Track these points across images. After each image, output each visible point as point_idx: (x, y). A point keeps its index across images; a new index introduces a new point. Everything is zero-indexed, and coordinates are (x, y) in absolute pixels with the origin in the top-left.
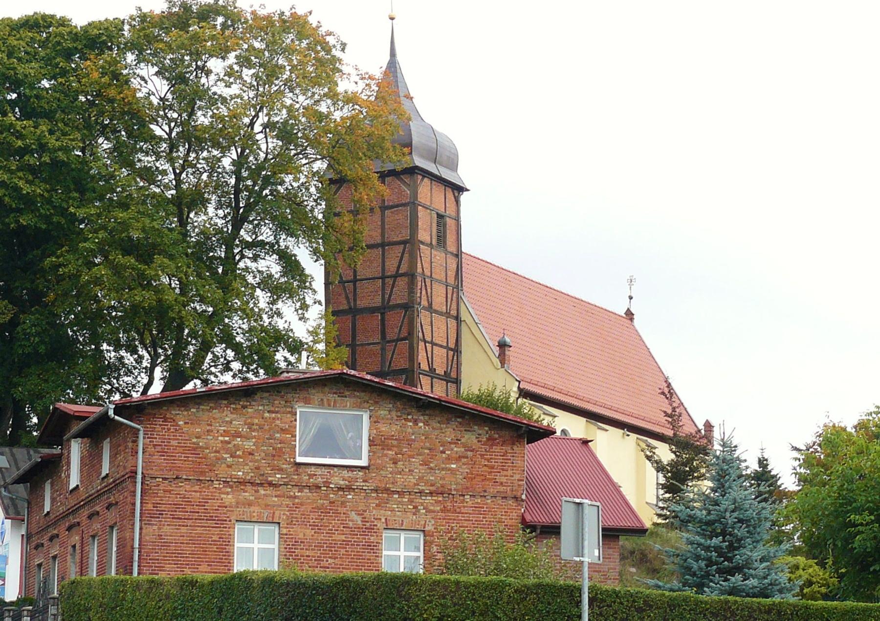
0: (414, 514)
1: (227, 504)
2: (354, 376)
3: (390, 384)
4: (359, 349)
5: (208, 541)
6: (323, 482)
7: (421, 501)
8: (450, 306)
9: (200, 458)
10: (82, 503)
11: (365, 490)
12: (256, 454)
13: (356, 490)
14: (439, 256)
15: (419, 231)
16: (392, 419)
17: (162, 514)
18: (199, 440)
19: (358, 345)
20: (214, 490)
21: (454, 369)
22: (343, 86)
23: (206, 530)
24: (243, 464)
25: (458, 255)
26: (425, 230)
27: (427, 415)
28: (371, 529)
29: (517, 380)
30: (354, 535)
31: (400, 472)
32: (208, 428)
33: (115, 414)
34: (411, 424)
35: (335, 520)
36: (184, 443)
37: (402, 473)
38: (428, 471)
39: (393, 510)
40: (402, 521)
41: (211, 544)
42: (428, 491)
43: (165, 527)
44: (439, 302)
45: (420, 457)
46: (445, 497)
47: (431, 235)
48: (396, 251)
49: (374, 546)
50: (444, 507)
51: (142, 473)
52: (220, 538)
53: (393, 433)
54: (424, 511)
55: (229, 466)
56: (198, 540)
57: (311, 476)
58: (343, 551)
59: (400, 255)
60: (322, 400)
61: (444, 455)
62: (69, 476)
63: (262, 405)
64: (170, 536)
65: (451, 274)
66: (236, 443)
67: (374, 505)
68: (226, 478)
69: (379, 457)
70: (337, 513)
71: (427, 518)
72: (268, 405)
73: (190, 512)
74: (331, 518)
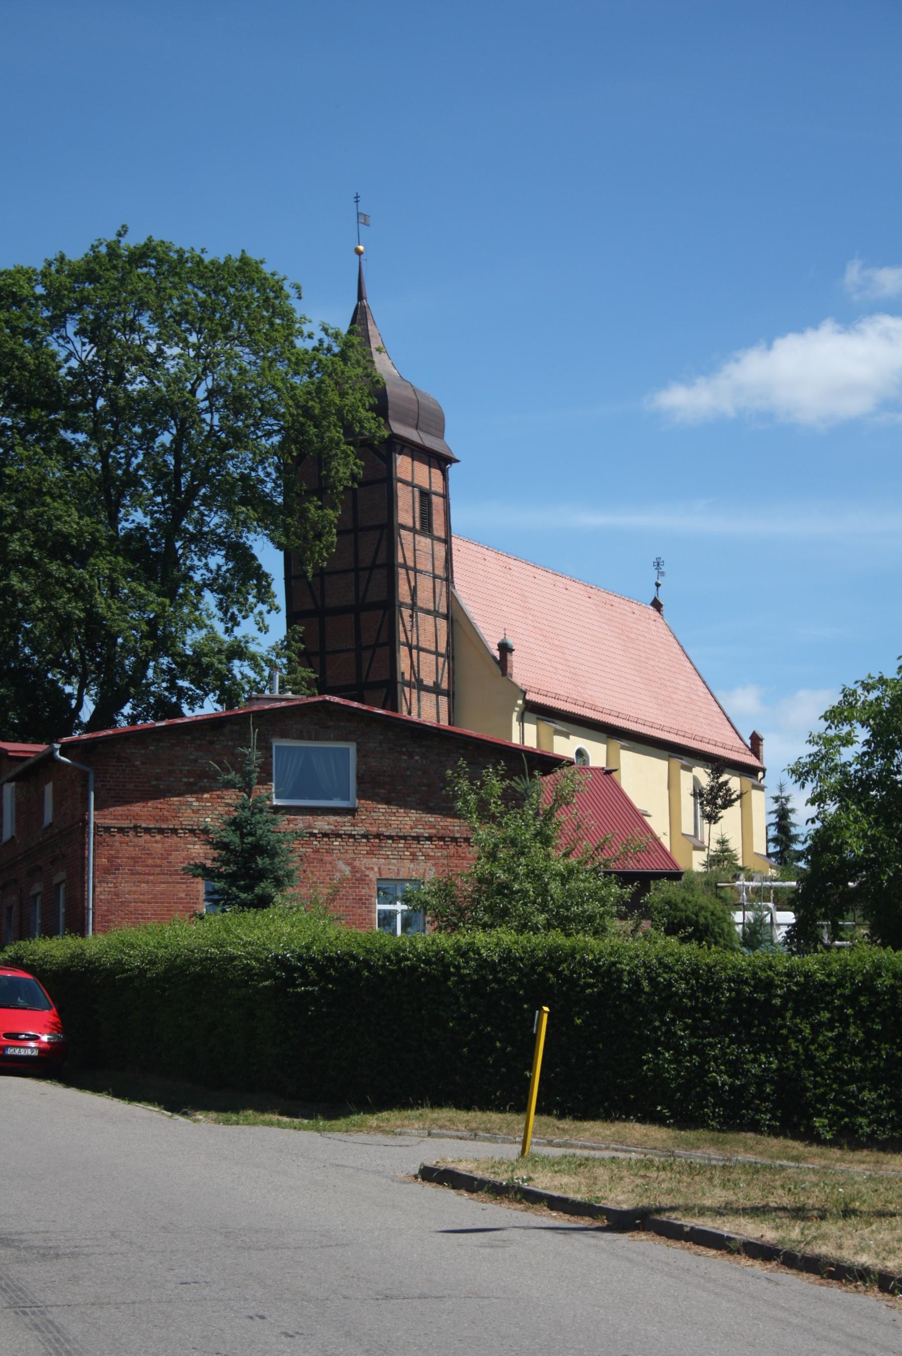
0: (412, 860)
2: (338, 704)
10: (19, 858)
14: (424, 542)
24: (212, 808)
26: (407, 511)
32: (169, 768)
34: (405, 757)
37: (397, 814)
41: (176, 903)
42: (427, 835)
47: (414, 517)
54: (423, 858)
55: (195, 812)
66: (202, 784)
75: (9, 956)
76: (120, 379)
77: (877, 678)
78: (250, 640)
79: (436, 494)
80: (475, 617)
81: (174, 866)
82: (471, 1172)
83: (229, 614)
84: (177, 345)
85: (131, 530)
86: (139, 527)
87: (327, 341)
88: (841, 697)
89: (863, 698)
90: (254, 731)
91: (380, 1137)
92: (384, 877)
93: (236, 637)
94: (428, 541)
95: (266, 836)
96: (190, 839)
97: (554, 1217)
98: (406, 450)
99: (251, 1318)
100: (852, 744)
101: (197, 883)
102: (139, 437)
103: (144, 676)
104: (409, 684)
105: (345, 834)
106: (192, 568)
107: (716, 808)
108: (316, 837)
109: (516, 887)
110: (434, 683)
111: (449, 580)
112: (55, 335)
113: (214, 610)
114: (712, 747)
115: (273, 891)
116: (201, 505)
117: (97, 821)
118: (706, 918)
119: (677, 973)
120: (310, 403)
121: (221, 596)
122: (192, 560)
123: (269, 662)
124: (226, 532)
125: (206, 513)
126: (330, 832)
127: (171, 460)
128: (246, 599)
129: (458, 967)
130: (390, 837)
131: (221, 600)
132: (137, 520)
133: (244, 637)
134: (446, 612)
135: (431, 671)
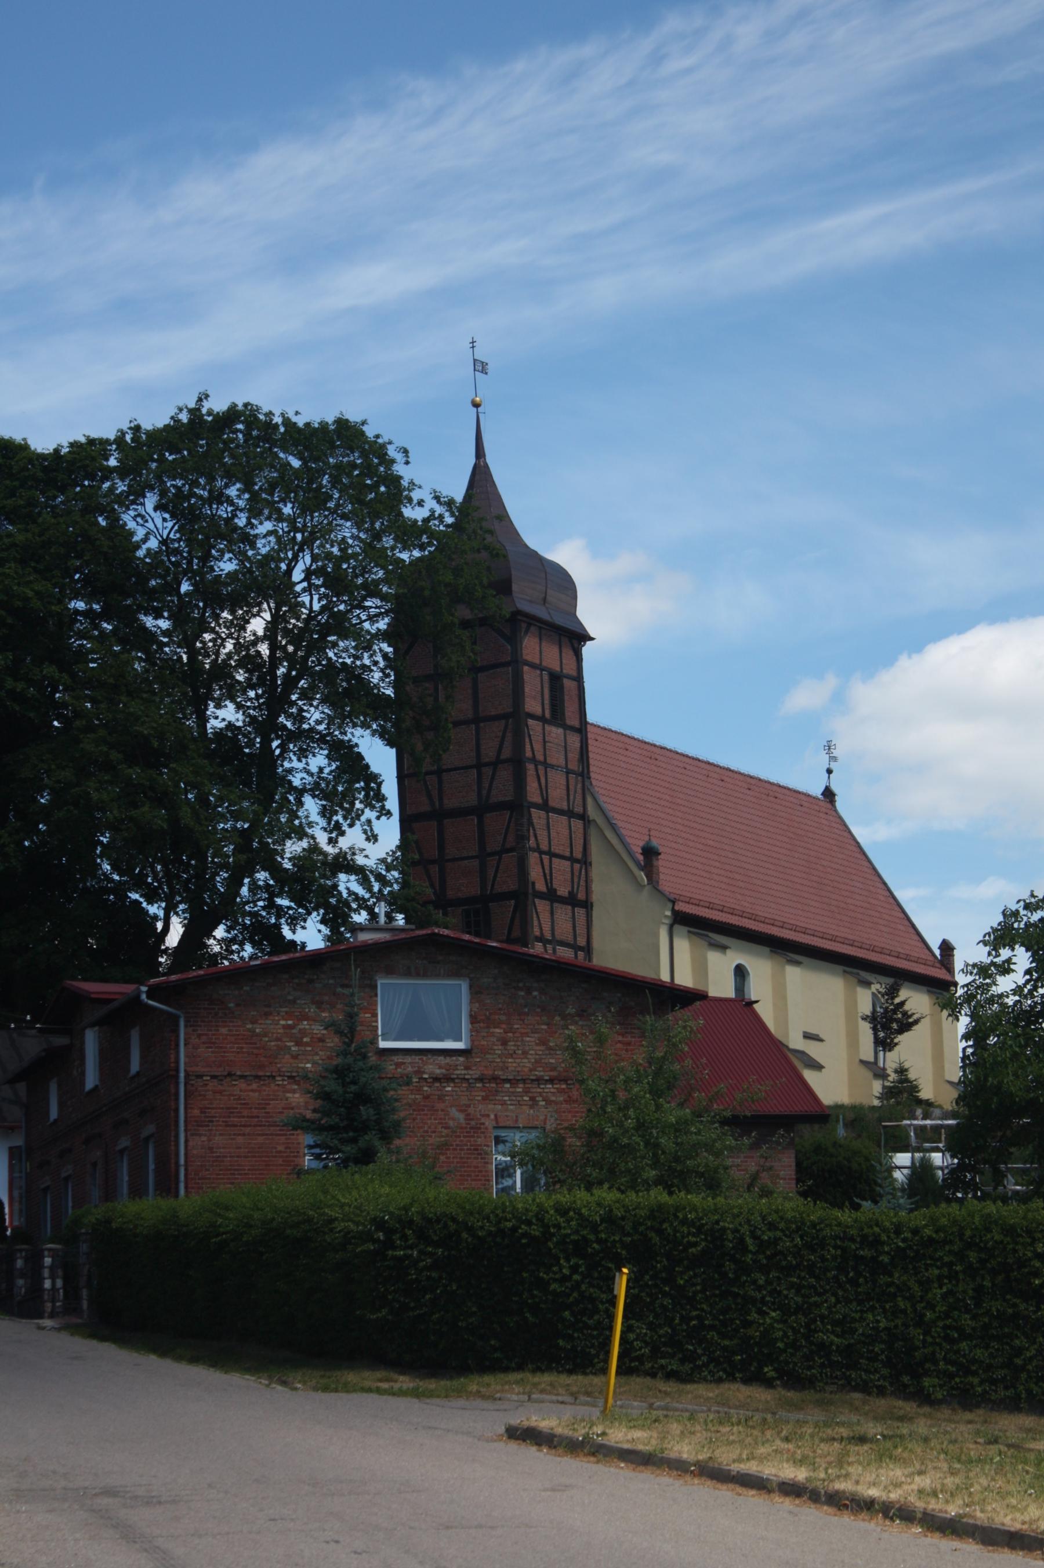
0: (531, 1107)
1: (294, 1104)
2: (447, 937)
3: (494, 944)
7: (539, 1090)
8: (574, 802)
10: (104, 1109)
12: (327, 1040)
13: (457, 1081)
14: (555, 733)
15: (527, 700)
17: (212, 1121)
18: (255, 1026)
19: (449, 860)
20: (276, 1088)
21: (582, 889)
25: (582, 727)
29: (670, 900)
31: (512, 1055)
33: (148, 997)
34: (522, 993)
35: (430, 1119)
36: (236, 1031)
37: (514, 1056)
38: (547, 1052)
39: (504, 1103)
40: (517, 1117)
41: (276, 1157)
42: (547, 1078)
43: (217, 1138)
44: (557, 796)
45: (536, 1035)
46: (570, 1084)
50: (569, 1097)
51: (185, 1071)
53: (500, 1006)
54: (544, 1103)
55: (295, 1057)
57: (398, 1065)
59: (501, 734)
62: (83, 1074)
64: (224, 1148)
65: (574, 756)
67: (480, 1098)
68: (291, 1072)
73: (248, 1117)
75: (97, 1219)
76: (206, 557)
78: (357, 852)
80: (616, 816)
81: (272, 1117)
82: (552, 1429)
83: (333, 823)
84: (269, 518)
85: (221, 729)
86: (230, 726)
87: (439, 510)
88: (1001, 918)
89: (1025, 919)
90: (356, 970)
91: (479, 1403)
92: (501, 1125)
93: (341, 849)
94: (560, 731)
95: (370, 1084)
96: (288, 1087)
97: (622, 1468)
98: (532, 628)
99: (327, 1542)
100: (1008, 973)
101: (298, 1135)
102: (229, 625)
103: (238, 894)
104: (541, 896)
105: (458, 1078)
106: (290, 771)
107: (892, 1033)
108: (427, 1082)
109: (626, 1141)
110: (569, 892)
111: (584, 774)
112: (132, 513)
113: (315, 817)
115: (377, 1143)
116: (299, 699)
117: (189, 1069)
118: (860, 1164)
119: (782, 1231)
121: (324, 803)
122: (291, 760)
123: (380, 878)
125: (305, 708)
126: (441, 1076)
127: (264, 649)
128: (353, 804)
129: (558, 1226)
130: (508, 1081)
131: (324, 806)
132: (228, 719)
133: (350, 848)
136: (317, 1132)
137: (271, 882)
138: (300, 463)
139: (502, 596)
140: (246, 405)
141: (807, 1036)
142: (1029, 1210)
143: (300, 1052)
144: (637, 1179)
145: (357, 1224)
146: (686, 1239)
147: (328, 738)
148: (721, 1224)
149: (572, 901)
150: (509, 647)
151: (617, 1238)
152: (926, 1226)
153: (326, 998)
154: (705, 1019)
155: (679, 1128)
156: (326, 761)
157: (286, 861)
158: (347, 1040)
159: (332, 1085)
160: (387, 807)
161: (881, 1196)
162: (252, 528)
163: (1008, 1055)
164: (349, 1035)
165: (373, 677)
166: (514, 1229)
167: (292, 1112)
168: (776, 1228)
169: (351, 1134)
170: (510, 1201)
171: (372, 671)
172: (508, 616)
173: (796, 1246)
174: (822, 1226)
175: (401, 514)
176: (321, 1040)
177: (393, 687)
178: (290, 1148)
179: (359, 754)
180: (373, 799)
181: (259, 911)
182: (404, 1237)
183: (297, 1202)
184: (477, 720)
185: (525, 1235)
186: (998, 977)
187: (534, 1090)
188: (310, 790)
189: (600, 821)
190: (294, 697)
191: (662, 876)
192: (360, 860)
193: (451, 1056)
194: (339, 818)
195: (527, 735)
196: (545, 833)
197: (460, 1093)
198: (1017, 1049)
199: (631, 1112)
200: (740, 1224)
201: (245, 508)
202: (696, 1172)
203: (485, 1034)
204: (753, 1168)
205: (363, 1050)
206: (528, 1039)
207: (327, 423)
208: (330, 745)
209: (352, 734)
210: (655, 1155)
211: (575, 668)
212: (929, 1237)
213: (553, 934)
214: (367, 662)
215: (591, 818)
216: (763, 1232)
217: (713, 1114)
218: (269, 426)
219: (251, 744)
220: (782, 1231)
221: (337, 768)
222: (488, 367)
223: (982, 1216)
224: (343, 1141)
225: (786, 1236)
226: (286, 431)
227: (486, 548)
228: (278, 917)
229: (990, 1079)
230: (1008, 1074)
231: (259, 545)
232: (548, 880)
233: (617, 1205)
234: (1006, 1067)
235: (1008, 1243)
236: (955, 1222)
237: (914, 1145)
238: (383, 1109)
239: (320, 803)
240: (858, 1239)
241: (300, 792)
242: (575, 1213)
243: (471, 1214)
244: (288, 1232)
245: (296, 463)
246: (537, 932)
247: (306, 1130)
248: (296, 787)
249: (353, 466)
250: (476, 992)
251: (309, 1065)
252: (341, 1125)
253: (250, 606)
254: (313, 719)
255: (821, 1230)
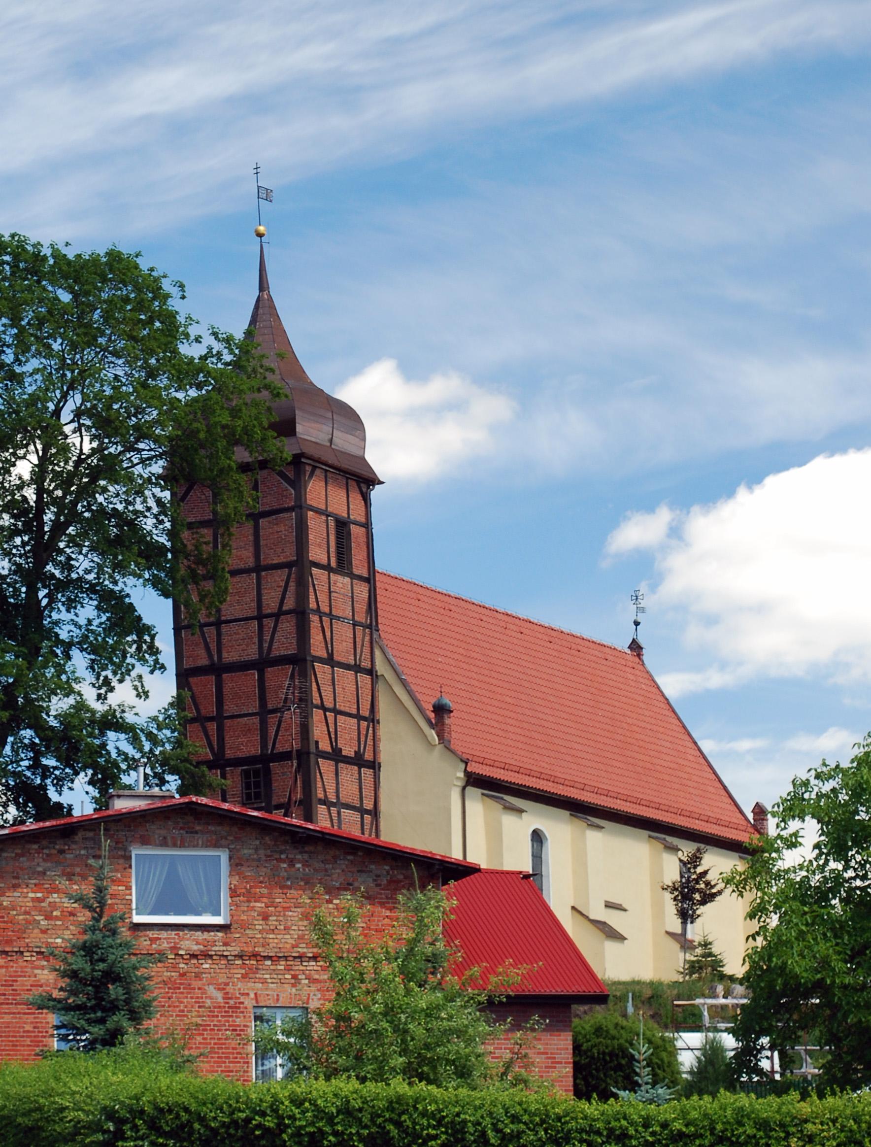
0: (294, 985)
1: (43, 981)
2: (206, 805)
4: (228, 723)
5: (19, 1032)
6: (171, 948)
7: (301, 968)
8: (361, 656)
9: (4, 922)
11: (227, 956)
12: (79, 914)
13: (214, 957)
14: (342, 582)
16: (259, 860)
20: (25, 964)
21: (369, 748)
22: (190, 350)
23: (16, 1018)
24: (63, 927)
25: (370, 579)
26: (320, 546)
27: (306, 852)
28: (236, 1008)
29: (462, 760)
30: (213, 1016)
34: (285, 866)
35: (187, 997)
39: (264, 982)
41: (23, 1037)
42: (311, 955)
44: (343, 651)
45: (299, 910)
48: (277, 579)
49: (241, 1030)
52: (35, 1027)
53: (261, 879)
54: (307, 981)
55: (44, 932)
56: (5, 1032)
57: (153, 940)
58: (199, 1039)
59: (283, 583)
60: (165, 838)
61: (331, 906)
63: (85, 848)
65: (361, 606)
67: (239, 976)
69: (243, 912)
70: (189, 987)
71: (311, 991)
72: (92, 848)
74: (181, 996)
77: (833, 766)
78: (127, 709)
79: (356, 523)
83: (102, 678)
87: (217, 346)
89: (816, 789)
90: (106, 841)
92: (260, 1004)
94: (347, 580)
98: (318, 472)
100: (796, 847)
101: (46, 1014)
106: (57, 623)
107: (693, 903)
110: (355, 752)
111: (372, 626)
114: (703, 823)
116: (68, 546)
119: (525, 1123)
120: (195, 425)
121: (93, 657)
123: (150, 736)
124: (98, 578)
125: (74, 556)
126: (198, 953)
127: (30, 493)
129: (292, 1118)
131: (93, 661)
134: (369, 666)
135: (351, 739)
136: (63, 1012)
137: (37, 741)
138: (71, 296)
139: (283, 438)
140: (13, 236)
141: (609, 905)
142: (783, 1103)
143: (50, 927)
144: (384, 1066)
145: (87, 1113)
146: (425, 1132)
147: (98, 588)
148: (462, 1116)
149: (358, 761)
150: (293, 492)
151: (354, 1131)
152: (674, 1120)
153: (78, 870)
154: (458, 899)
155: (430, 1013)
156: (95, 613)
157: (52, 718)
158: (96, 915)
159: (79, 963)
160: (161, 661)
161: (640, 1086)
162: (19, 365)
163: (793, 934)
164: (98, 910)
165: (145, 524)
166: (248, 1120)
167: (41, 989)
168: (520, 1121)
169: (99, 1014)
170: (245, 1092)
171: (146, 517)
172: (289, 459)
173: (540, 1139)
174: (568, 1118)
175: (175, 352)
176: (72, 914)
177: (166, 535)
178: (38, 1028)
179: (131, 604)
180: (146, 652)
181: (23, 771)
182: (135, 1128)
183: (29, 1089)
184: (258, 569)
185: (259, 1126)
186: (784, 850)
187: (297, 968)
188: (78, 643)
189: (389, 676)
190: (62, 545)
191: (454, 735)
192: (130, 718)
193: (209, 931)
194: (109, 673)
195: (311, 585)
196: (330, 689)
197: (218, 971)
198: (804, 928)
199: (379, 997)
200: (482, 1117)
201: (12, 344)
202: (447, 1060)
203: (246, 909)
204: (508, 1055)
205: (112, 926)
206: (290, 913)
207: (99, 255)
208: (100, 596)
209: (124, 583)
210: (404, 1041)
211: (363, 514)
212: (679, 1131)
213: (338, 797)
214: (139, 507)
215: (379, 674)
216: (506, 1125)
217: (466, 999)
218: (38, 258)
219: (17, 591)
220: (525, 1123)
221: (108, 619)
222: (273, 194)
223: (734, 1110)
224: (90, 1022)
225: (529, 1129)
226: (55, 262)
227: (267, 387)
228: (44, 777)
229: (774, 959)
230: (793, 954)
231: (27, 384)
232: (333, 738)
233: (355, 1096)
234: (792, 948)
235: (761, 1138)
236: (706, 1115)
237: (707, 1025)
238: (133, 988)
239: (89, 657)
240: (605, 1133)
241: (68, 646)
242: (311, 1104)
243: (204, 1104)
244: (19, 1120)
245: (65, 297)
246: (320, 795)
247: (53, 1009)
248: (63, 641)
249: (126, 300)
250: (236, 864)
251: (59, 941)
252: (89, 1005)
253: (17, 447)
254: (82, 568)
255: (566, 1123)
